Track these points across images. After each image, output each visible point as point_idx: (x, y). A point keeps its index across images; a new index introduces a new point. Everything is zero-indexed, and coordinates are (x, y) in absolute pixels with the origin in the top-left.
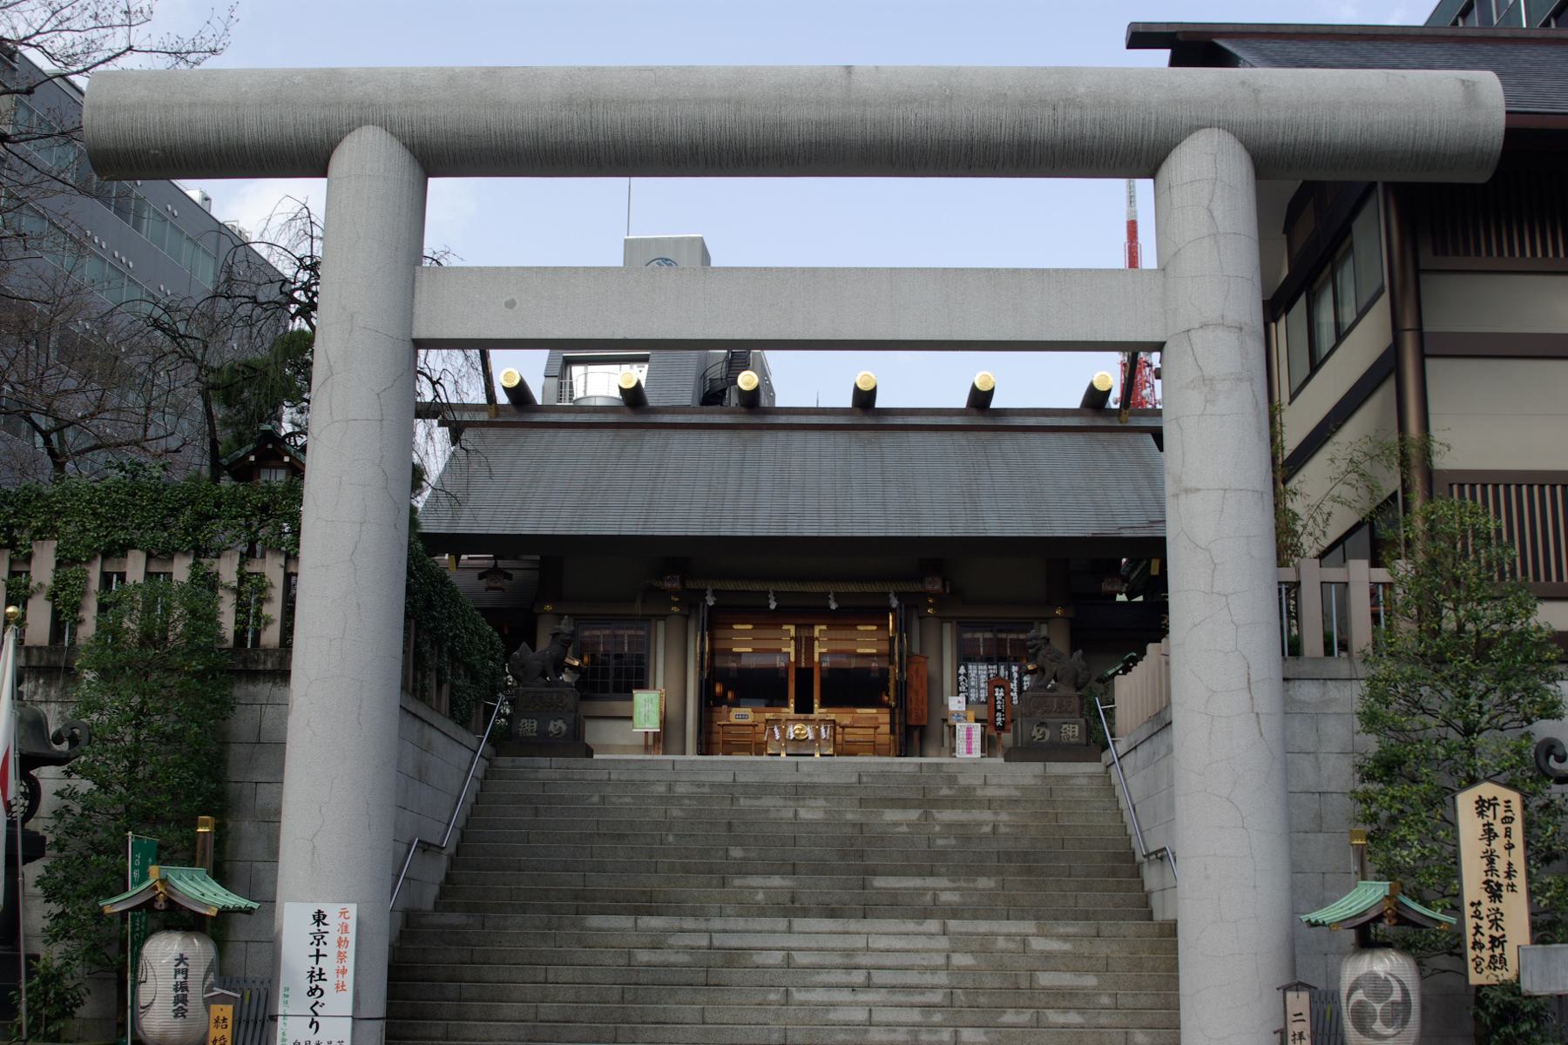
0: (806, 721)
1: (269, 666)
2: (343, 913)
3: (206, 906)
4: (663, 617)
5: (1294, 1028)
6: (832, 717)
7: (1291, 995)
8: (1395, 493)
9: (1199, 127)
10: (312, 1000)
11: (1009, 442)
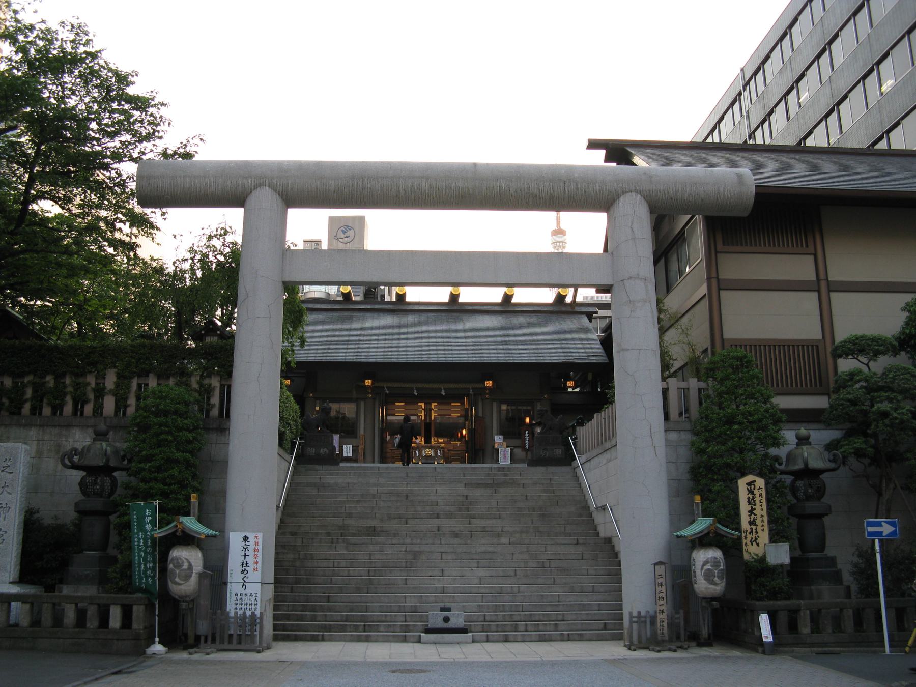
0: (431, 447)
1: (214, 426)
2: (256, 537)
3: (200, 534)
4: (364, 399)
5: (660, 581)
7: (657, 567)
8: (707, 349)
9: (627, 192)
10: (243, 575)
11: (521, 319)
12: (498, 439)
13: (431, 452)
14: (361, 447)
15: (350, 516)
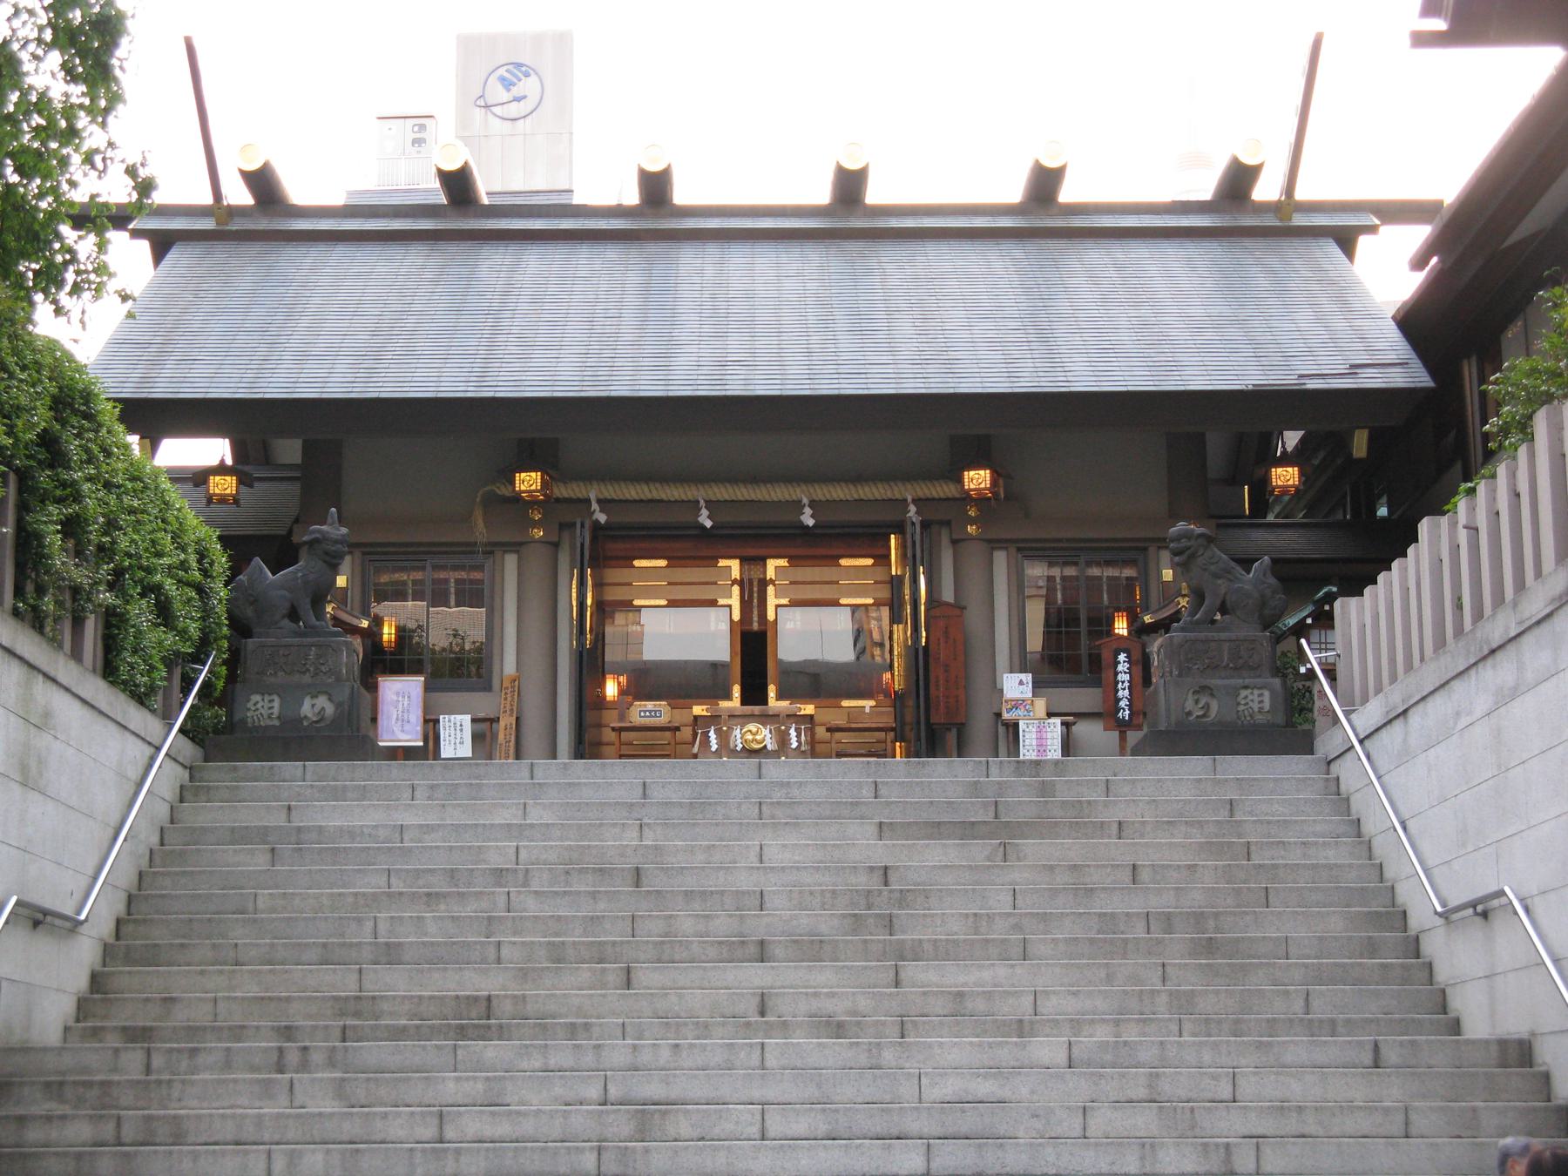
0: (765, 719)
4: (516, 547)
6: (809, 709)
11: (1096, 256)
12: (1016, 685)
13: (764, 735)
14: (507, 721)
15: (391, 954)
